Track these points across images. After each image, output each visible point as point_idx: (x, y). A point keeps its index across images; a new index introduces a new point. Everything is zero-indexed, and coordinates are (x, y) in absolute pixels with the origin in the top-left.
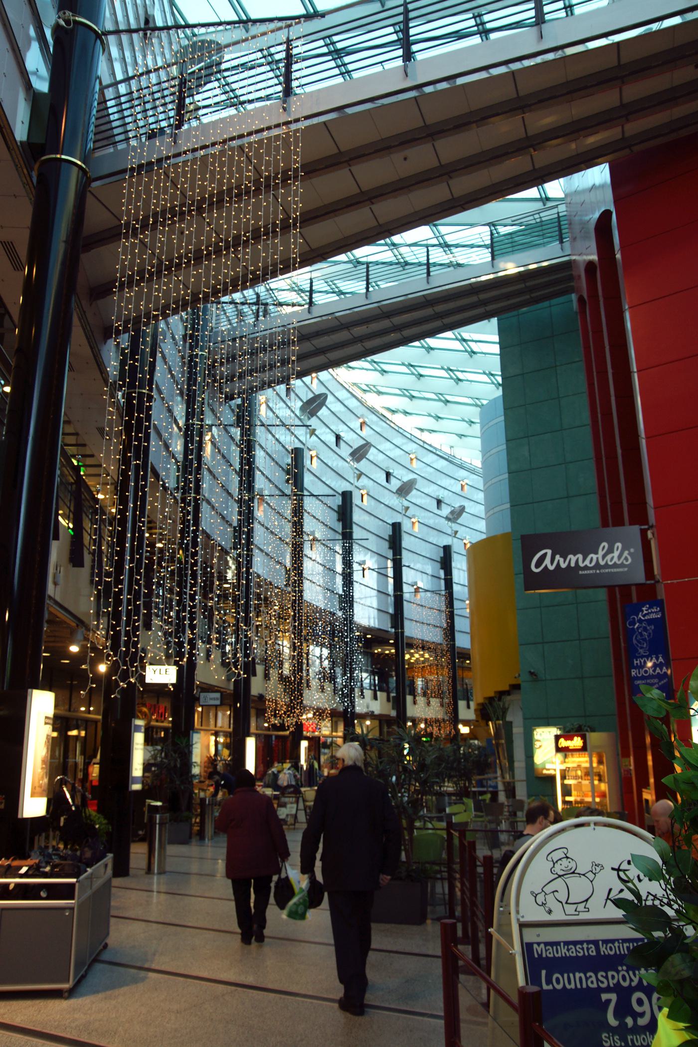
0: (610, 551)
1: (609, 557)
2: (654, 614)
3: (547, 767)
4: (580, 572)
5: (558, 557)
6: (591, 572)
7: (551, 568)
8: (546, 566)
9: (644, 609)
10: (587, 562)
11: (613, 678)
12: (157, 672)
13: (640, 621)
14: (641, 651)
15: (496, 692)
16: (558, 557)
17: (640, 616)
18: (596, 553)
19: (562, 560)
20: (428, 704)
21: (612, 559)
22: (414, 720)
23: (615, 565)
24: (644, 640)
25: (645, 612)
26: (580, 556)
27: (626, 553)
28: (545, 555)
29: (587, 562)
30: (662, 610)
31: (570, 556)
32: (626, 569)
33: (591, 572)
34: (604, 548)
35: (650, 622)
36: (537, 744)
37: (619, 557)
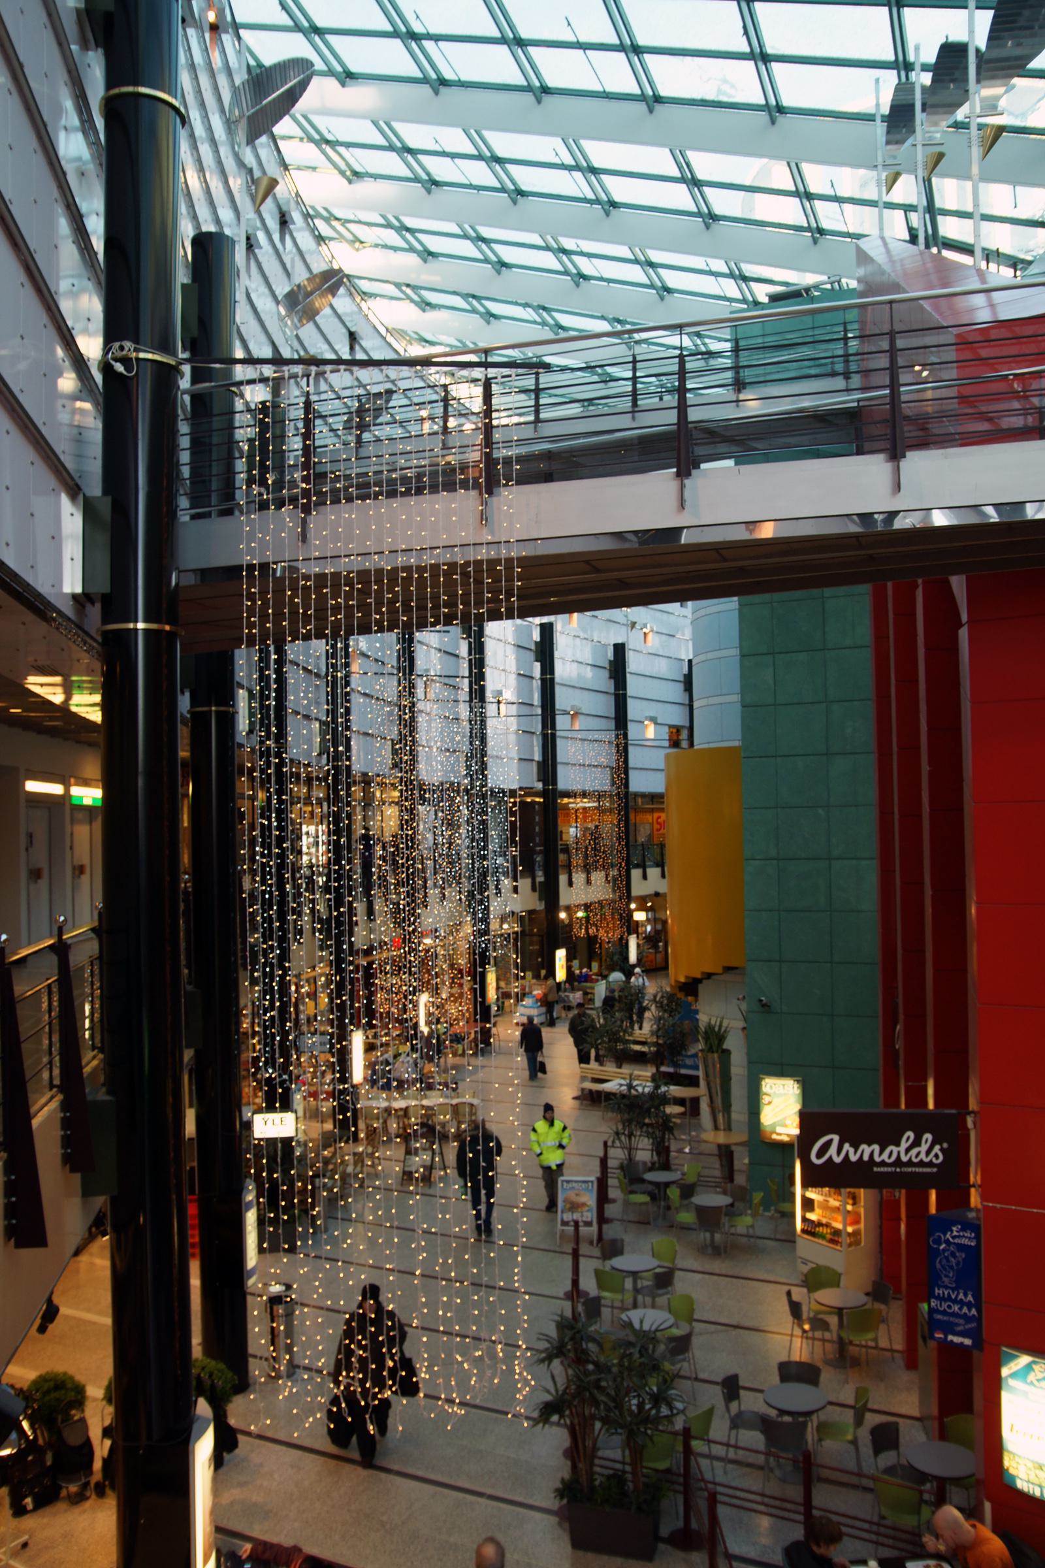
0: (917, 1143)
1: (914, 1152)
2: (967, 1239)
3: (779, 1130)
4: (875, 1169)
5: (847, 1146)
6: (889, 1169)
7: (838, 1160)
8: (830, 1157)
9: (954, 1229)
10: (885, 1156)
11: (880, 1020)
12: (270, 1123)
13: (947, 1242)
14: (946, 1280)
15: (703, 973)
16: (847, 1146)
17: (948, 1236)
18: (898, 1144)
19: (852, 1150)
20: (589, 882)
21: (918, 1154)
22: (568, 909)
23: (921, 1164)
24: (951, 1267)
25: (955, 1233)
26: (876, 1147)
27: (937, 1148)
28: (830, 1142)
29: (885, 1156)
30: (978, 1238)
31: (864, 1147)
32: (935, 1170)
33: (889, 1169)
34: (908, 1138)
35: (961, 1247)
36: (765, 1099)
37: (928, 1153)
